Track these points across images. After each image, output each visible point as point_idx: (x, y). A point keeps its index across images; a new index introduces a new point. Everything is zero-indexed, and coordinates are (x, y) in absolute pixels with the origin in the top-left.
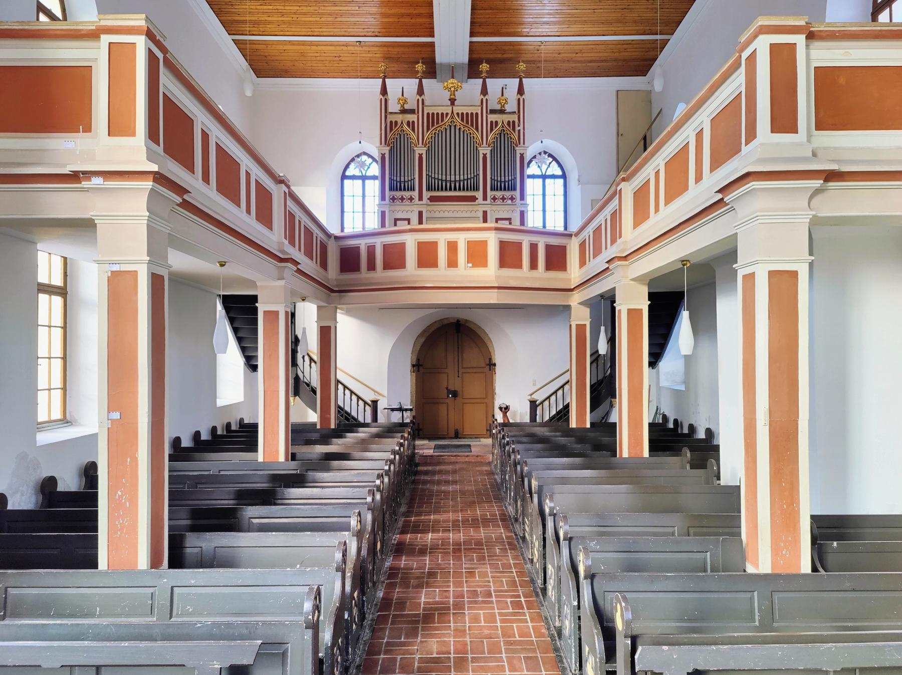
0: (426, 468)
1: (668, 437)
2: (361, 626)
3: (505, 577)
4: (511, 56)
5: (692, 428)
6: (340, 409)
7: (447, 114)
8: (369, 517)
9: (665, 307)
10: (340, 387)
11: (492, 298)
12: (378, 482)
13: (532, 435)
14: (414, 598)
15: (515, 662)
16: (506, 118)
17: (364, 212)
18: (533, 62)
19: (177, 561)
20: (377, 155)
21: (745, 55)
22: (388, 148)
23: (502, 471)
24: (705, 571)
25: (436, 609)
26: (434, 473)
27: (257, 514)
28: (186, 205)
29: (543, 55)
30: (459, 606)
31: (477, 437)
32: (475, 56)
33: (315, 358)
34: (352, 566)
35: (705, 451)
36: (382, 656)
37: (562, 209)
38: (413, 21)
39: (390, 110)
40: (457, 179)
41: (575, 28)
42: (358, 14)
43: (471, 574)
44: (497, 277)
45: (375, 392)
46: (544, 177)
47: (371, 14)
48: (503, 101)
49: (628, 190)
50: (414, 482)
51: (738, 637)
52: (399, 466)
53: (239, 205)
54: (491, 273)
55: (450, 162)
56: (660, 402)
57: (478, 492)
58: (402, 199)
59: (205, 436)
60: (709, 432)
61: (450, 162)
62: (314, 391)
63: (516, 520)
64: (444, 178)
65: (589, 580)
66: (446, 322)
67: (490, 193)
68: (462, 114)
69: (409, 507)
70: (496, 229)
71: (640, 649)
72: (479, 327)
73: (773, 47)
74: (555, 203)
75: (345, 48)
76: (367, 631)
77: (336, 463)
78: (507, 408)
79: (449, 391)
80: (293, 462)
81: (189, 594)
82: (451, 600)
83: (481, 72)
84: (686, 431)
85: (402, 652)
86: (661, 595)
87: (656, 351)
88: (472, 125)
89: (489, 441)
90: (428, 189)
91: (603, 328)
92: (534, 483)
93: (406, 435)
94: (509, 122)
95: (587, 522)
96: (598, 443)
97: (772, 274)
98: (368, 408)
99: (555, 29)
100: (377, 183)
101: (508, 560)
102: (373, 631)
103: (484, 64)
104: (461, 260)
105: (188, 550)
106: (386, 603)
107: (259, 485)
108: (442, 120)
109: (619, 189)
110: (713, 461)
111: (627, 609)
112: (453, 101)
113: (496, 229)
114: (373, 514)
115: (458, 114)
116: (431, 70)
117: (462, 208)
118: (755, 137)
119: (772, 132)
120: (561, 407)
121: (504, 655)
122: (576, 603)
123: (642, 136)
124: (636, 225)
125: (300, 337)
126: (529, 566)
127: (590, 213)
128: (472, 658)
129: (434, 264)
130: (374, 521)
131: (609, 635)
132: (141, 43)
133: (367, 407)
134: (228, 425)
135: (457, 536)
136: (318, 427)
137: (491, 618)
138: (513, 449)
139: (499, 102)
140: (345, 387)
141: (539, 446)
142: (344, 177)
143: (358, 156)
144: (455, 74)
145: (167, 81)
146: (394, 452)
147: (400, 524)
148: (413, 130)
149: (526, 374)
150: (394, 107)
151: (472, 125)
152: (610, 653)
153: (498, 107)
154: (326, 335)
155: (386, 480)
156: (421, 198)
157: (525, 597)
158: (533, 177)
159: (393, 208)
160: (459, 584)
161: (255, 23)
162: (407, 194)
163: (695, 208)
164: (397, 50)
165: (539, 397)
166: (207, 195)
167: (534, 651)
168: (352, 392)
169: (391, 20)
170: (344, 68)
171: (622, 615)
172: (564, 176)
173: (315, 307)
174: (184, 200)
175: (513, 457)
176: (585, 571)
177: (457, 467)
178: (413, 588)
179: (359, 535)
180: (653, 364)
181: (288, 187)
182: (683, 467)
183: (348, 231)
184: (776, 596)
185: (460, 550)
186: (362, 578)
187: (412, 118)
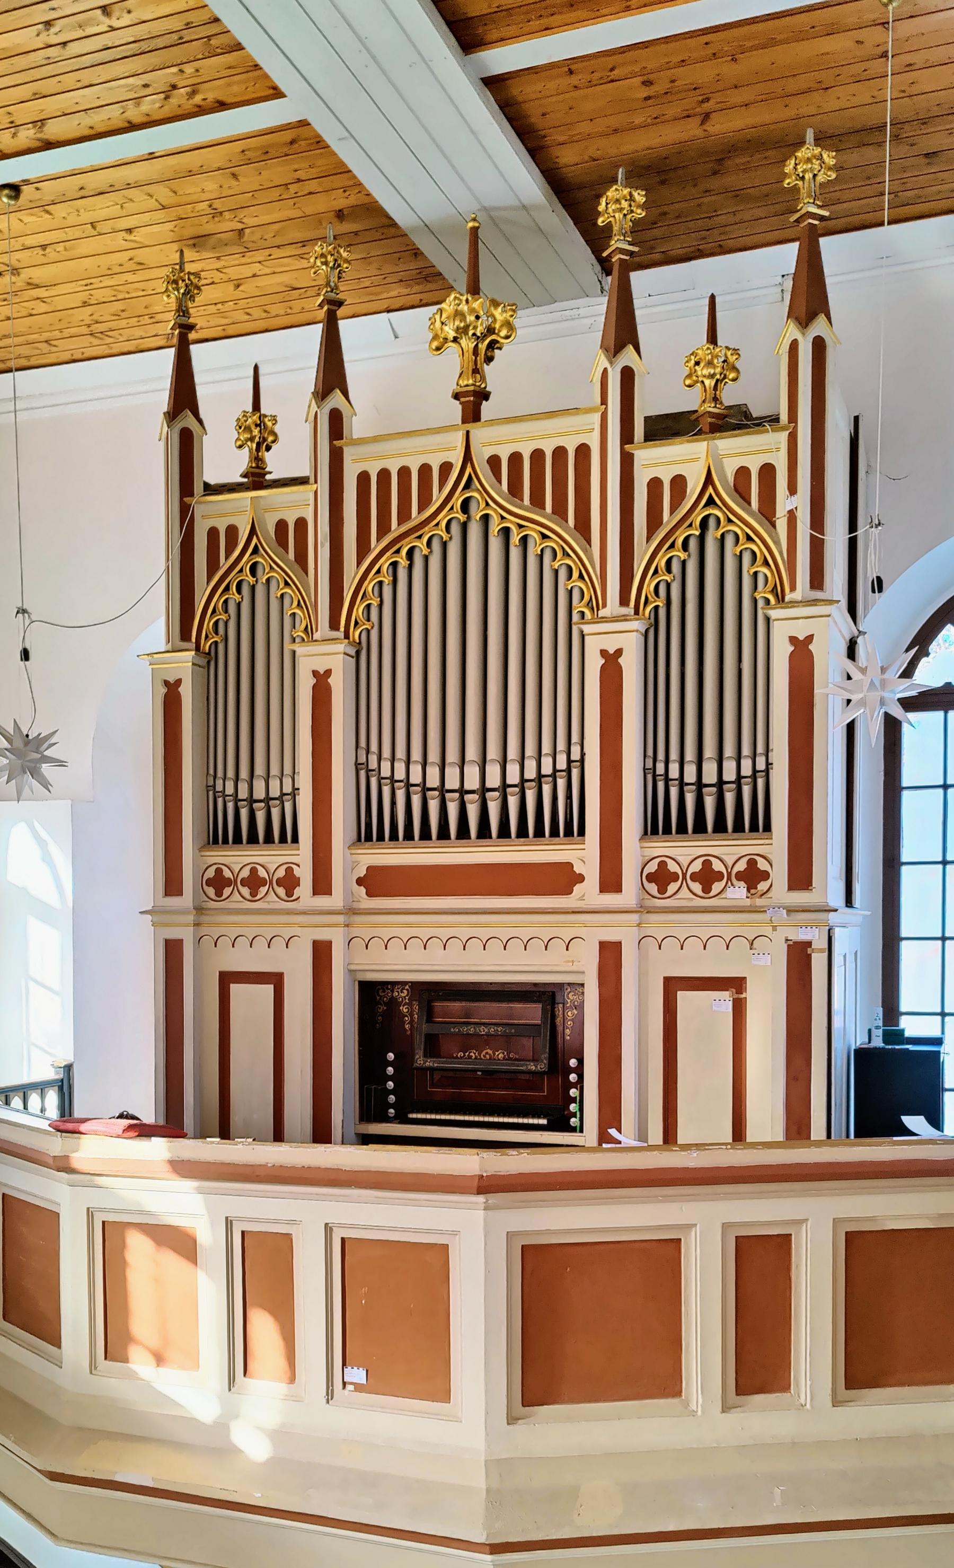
18: (548, 171)
22: (638, 625)
40: (493, 780)
58: (254, 882)
64: (433, 780)
67: (635, 851)
88: (560, 510)
108: (425, 501)
112: (473, 403)
115: (494, 462)
117: (527, 928)
139: (692, 381)
150: (222, 460)
151: (560, 510)
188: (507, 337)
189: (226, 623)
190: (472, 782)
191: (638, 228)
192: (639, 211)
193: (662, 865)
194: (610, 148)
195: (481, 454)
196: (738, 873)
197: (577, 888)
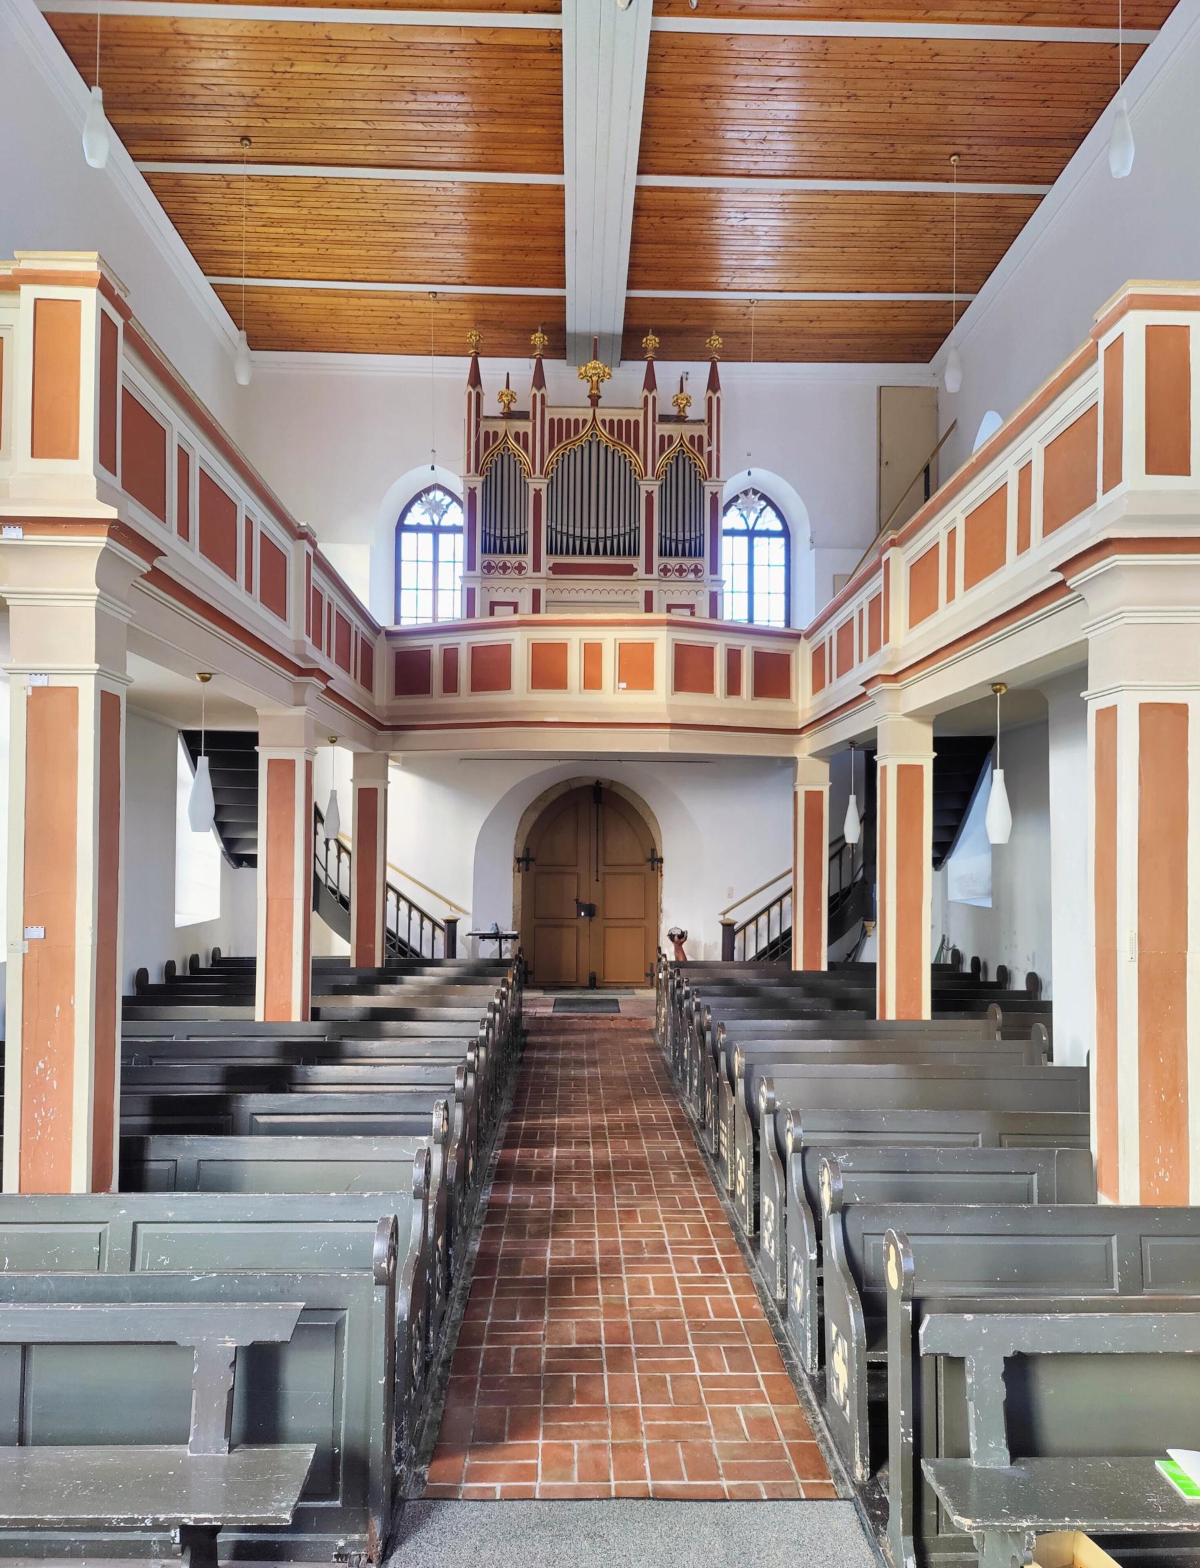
0: (540, 1039)
1: (964, 988)
2: (446, 1296)
3: (687, 1220)
4: (697, 323)
5: (1004, 973)
6: (390, 936)
7: (585, 421)
8: (458, 1114)
9: (961, 761)
10: (391, 896)
12: (470, 1056)
13: (727, 983)
14: (535, 1253)
15: (711, 1356)
16: (687, 431)
17: (435, 590)
18: (736, 334)
19: (134, 1178)
20: (459, 489)
21: (1104, 342)
22: (481, 479)
23: (675, 1043)
24: (1029, 1200)
25: (572, 1271)
26: (555, 1047)
27: (264, 1107)
28: (157, 577)
29: (753, 323)
30: (611, 1266)
31: (629, 986)
32: (635, 322)
33: (349, 845)
34: (435, 1193)
35: (1028, 1009)
36: (484, 1346)
37: (782, 589)
38: (530, 259)
39: (486, 411)
40: (601, 534)
41: (808, 279)
42: (433, 246)
43: (629, 1215)
45: (451, 904)
46: (751, 534)
47: (457, 246)
48: (681, 400)
49: (901, 561)
50: (521, 1061)
51: (1086, 1301)
52: (500, 1033)
53: (234, 576)
54: (660, 698)
55: (591, 504)
56: (947, 929)
57: (634, 1079)
58: (505, 568)
59: (154, 979)
60: (1033, 979)
61: (591, 504)
62: (345, 903)
63: (703, 1127)
64: (578, 533)
65: (839, 1215)
66: (576, 785)
67: (657, 561)
68: (612, 421)
69: (516, 1104)
70: (670, 623)
71: (927, 1319)
73: (1150, 329)
74: (771, 579)
75: (408, 303)
76: (456, 1306)
77: (391, 1026)
78: (683, 936)
79: (580, 906)
80: (317, 1023)
81: (163, 1236)
82: (598, 1257)
83: (645, 350)
84: (993, 977)
85: (518, 1339)
86: (958, 1240)
87: (944, 839)
89: (652, 994)
90: (550, 552)
91: (852, 798)
92: (738, 1061)
93: (510, 980)
94: (692, 437)
95: (829, 1125)
96: (842, 996)
97: (1145, 709)
98: (439, 934)
99: (773, 279)
100: (460, 540)
101: (692, 1192)
102: (467, 1305)
103: (651, 337)
104: (608, 674)
105: (153, 1166)
106: (485, 1262)
107: (260, 1061)
108: (577, 432)
109: (884, 558)
110: (1042, 1026)
111: (906, 1254)
112: (595, 400)
113: (670, 623)
114: (465, 1110)
115: (603, 422)
116: (558, 345)
117: (616, 586)
118: (1119, 480)
119: (1148, 472)
120: (776, 934)
121: (691, 1345)
122: (814, 1256)
123: (920, 466)
124: (914, 620)
125: (324, 810)
126: (727, 1202)
127: (831, 601)
128: (637, 1349)
129: (559, 683)
130: (466, 1119)
131: (874, 1309)
132: (89, 301)
133: (438, 932)
134: (194, 960)
135: (601, 1152)
136: (353, 964)
137: (666, 1286)
138: (698, 1005)
140: (400, 896)
141: (740, 1000)
142: (401, 527)
143: (427, 491)
144: (600, 355)
145: (128, 367)
146: (493, 1008)
147: (502, 1131)
148: (525, 448)
149: (716, 878)
150: (492, 407)
152: (876, 1332)
153: (674, 411)
154: (370, 806)
155: (482, 1054)
156: (537, 567)
157: (722, 1252)
158: (732, 533)
159: (488, 584)
160: (608, 1231)
161: (253, 256)
162: (512, 560)
163: (1021, 593)
164: (500, 307)
165: (739, 917)
166: (187, 559)
167: (741, 1338)
168: (411, 905)
169: (483, 257)
170: (405, 338)
171: (898, 1265)
172: (786, 533)
173: (351, 754)
174: (153, 567)
175: (696, 1018)
176: (832, 1199)
177: (596, 1036)
178: (531, 1236)
179: (445, 1141)
180: (938, 862)
181: (314, 545)
182: (990, 1037)
183: (407, 623)
184: (1149, 1243)
185: (607, 1176)
186: (449, 1216)
187: (523, 426)
190: (593, 535)
194: (649, 322)
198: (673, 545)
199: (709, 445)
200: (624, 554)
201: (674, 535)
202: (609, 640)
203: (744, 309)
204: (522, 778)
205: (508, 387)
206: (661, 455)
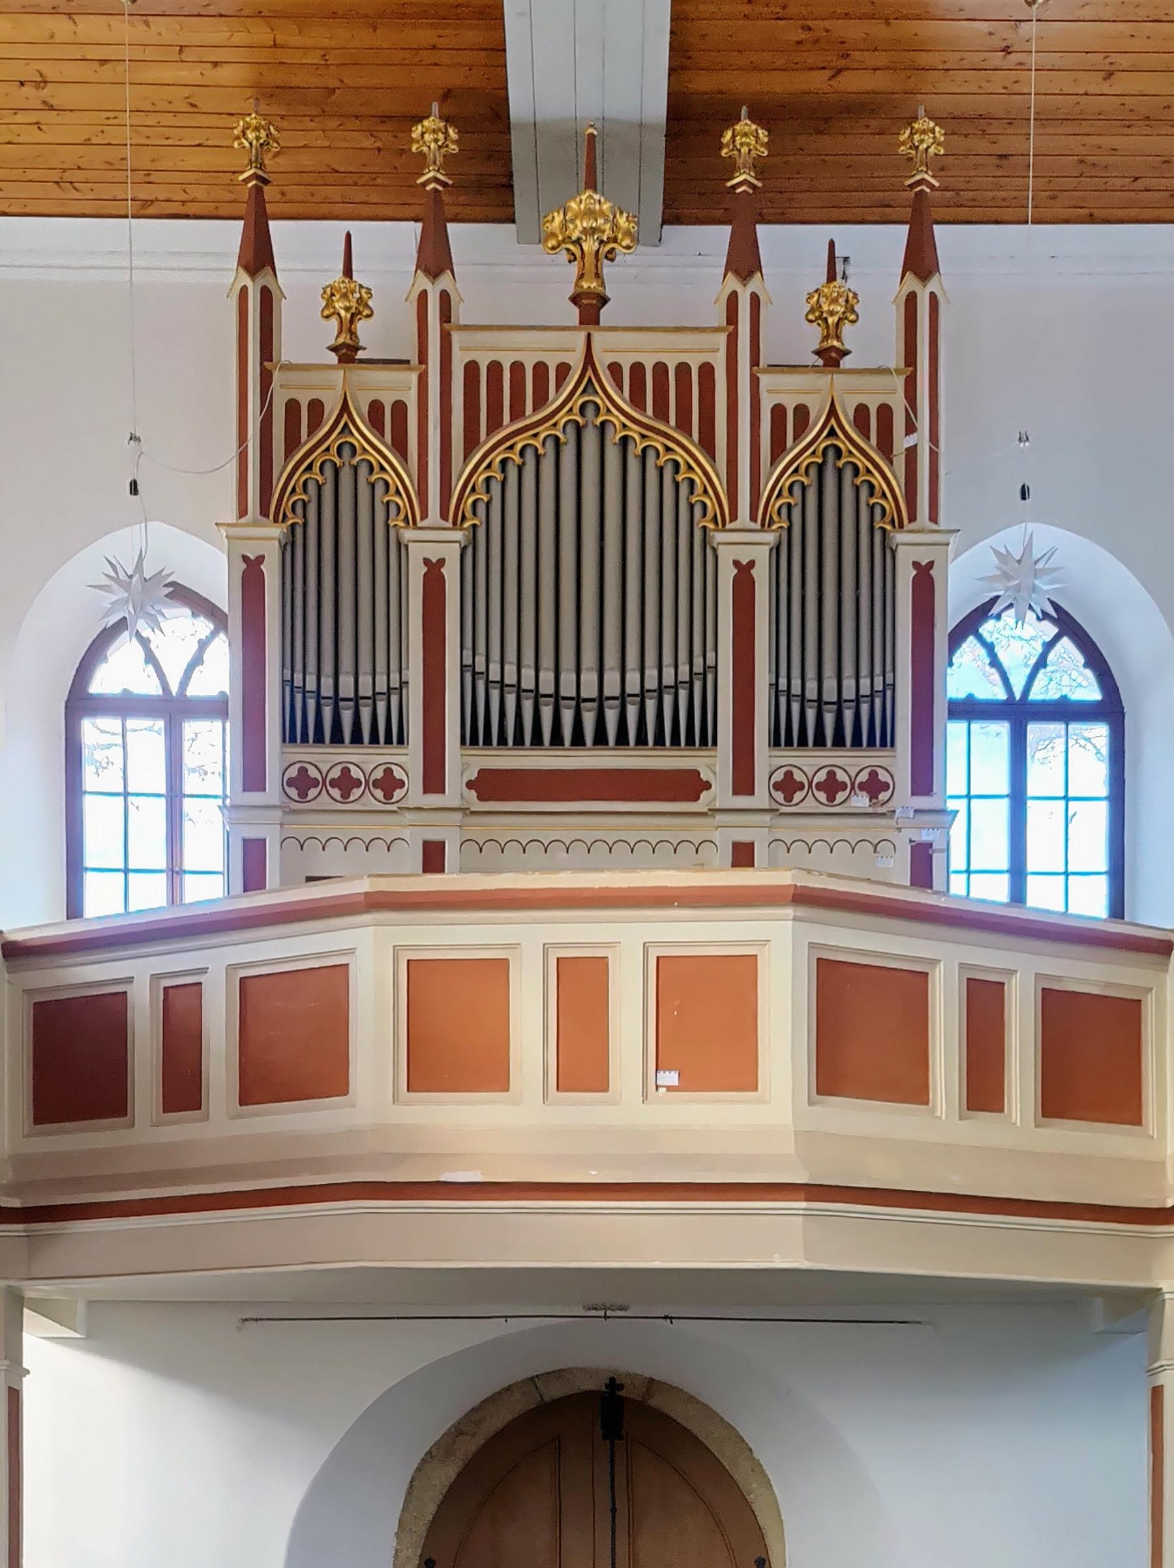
7: (563, 370)
11: (779, 1242)
20: (217, 579)
22: (277, 531)
32: (701, 83)
44: (805, 1138)
54: (773, 1113)
58: (346, 783)
64: (547, 687)
66: (554, 1391)
67: (768, 761)
70: (802, 898)
72: (710, 1414)
88: (684, 424)
90: (472, 738)
94: (861, 413)
103: (745, 125)
108: (541, 399)
112: (590, 305)
113: (802, 898)
129: (489, 1071)
142: (80, 703)
148: (400, 446)
150: (305, 337)
156: (434, 780)
158: (969, 710)
159: (301, 827)
162: (366, 760)
172: (1110, 709)
188: (628, 247)
189: (488, 504)
191: (760, 168)
192: (762, 149)
193: (789, 774)
195: (602, 361)
196: (861, 784)
197: (704, 795)
198: (811, 714)
199: (910, 429)
200: (675, 741)
201: (812, 686)
202: (629, 946)
203: (1005, 33)
204: (29, 973)
205: (348, 271)
206: (774, 460)
